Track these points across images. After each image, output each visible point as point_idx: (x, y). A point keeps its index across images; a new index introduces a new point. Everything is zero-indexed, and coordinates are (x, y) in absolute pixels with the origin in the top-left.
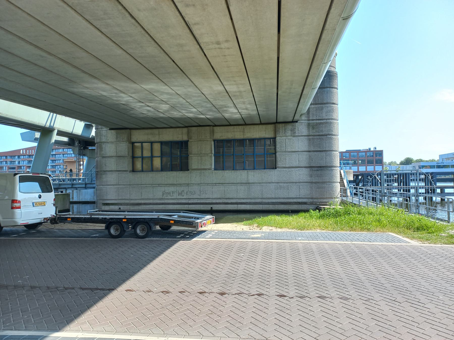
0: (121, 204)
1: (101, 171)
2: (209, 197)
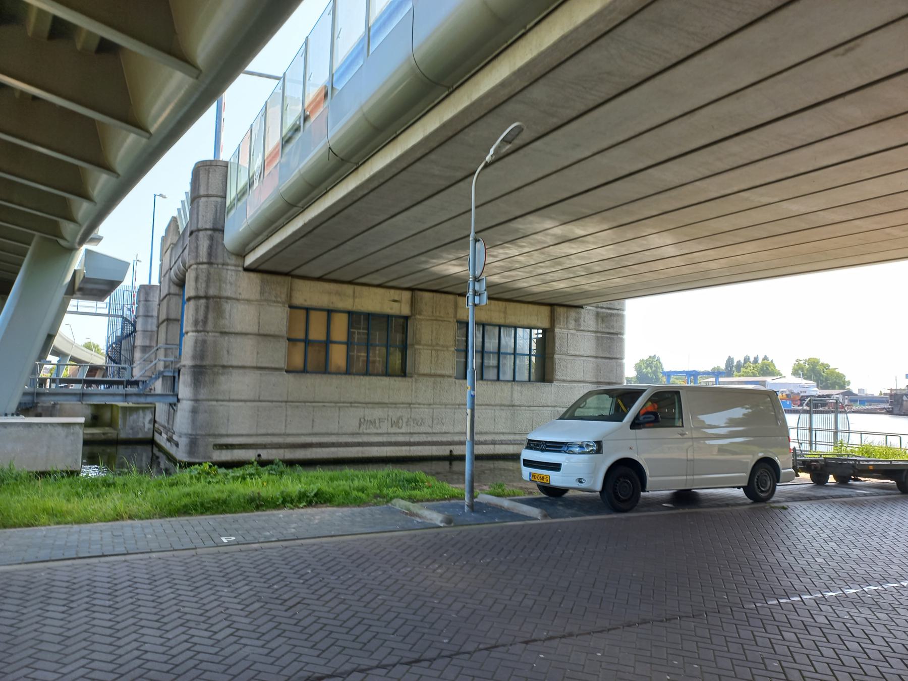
0: (264, 446)
1: (215, 366)
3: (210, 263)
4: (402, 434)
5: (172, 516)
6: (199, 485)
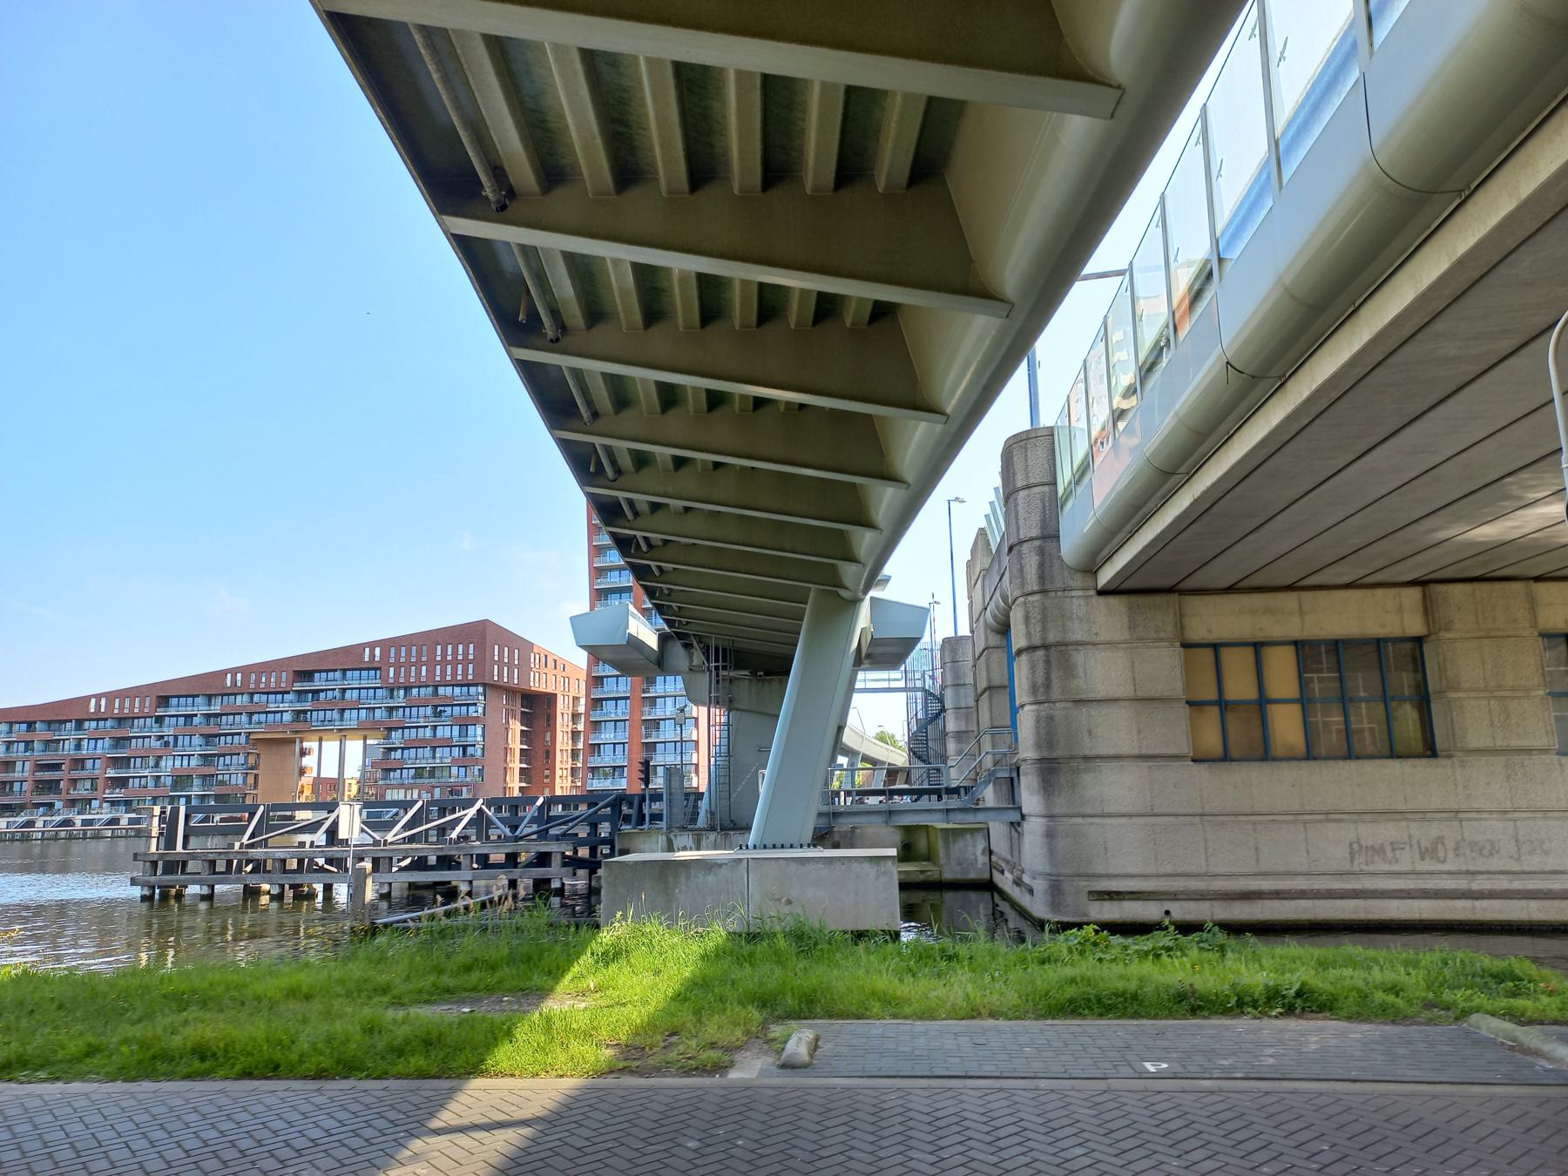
0: (1174, 896)
1: (1072, 758)
2: (1559, 868)
3: (1043, 592)
4: (1448, 873)
5: (1054, 1018)
6: (1084, 964)
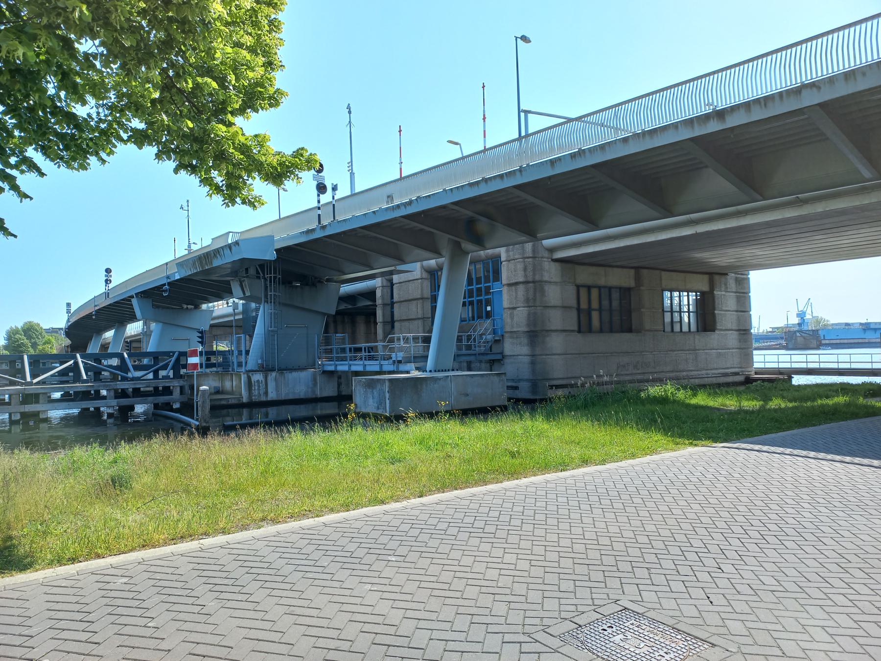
3: (534, 257)
4: (639, 374)
